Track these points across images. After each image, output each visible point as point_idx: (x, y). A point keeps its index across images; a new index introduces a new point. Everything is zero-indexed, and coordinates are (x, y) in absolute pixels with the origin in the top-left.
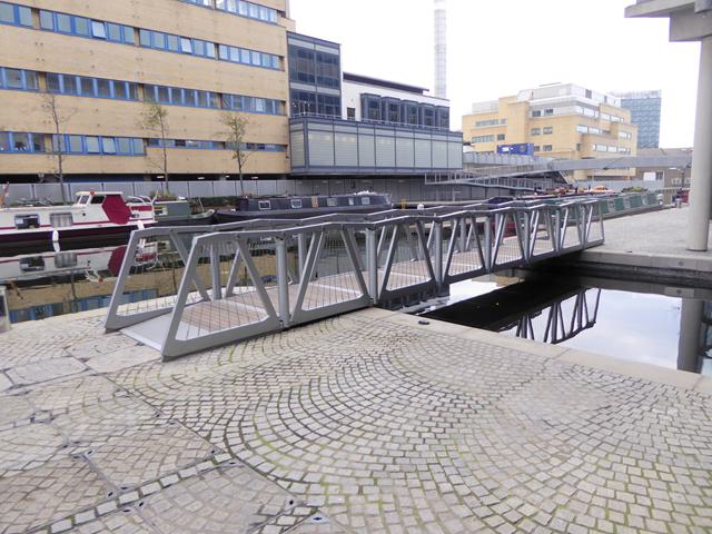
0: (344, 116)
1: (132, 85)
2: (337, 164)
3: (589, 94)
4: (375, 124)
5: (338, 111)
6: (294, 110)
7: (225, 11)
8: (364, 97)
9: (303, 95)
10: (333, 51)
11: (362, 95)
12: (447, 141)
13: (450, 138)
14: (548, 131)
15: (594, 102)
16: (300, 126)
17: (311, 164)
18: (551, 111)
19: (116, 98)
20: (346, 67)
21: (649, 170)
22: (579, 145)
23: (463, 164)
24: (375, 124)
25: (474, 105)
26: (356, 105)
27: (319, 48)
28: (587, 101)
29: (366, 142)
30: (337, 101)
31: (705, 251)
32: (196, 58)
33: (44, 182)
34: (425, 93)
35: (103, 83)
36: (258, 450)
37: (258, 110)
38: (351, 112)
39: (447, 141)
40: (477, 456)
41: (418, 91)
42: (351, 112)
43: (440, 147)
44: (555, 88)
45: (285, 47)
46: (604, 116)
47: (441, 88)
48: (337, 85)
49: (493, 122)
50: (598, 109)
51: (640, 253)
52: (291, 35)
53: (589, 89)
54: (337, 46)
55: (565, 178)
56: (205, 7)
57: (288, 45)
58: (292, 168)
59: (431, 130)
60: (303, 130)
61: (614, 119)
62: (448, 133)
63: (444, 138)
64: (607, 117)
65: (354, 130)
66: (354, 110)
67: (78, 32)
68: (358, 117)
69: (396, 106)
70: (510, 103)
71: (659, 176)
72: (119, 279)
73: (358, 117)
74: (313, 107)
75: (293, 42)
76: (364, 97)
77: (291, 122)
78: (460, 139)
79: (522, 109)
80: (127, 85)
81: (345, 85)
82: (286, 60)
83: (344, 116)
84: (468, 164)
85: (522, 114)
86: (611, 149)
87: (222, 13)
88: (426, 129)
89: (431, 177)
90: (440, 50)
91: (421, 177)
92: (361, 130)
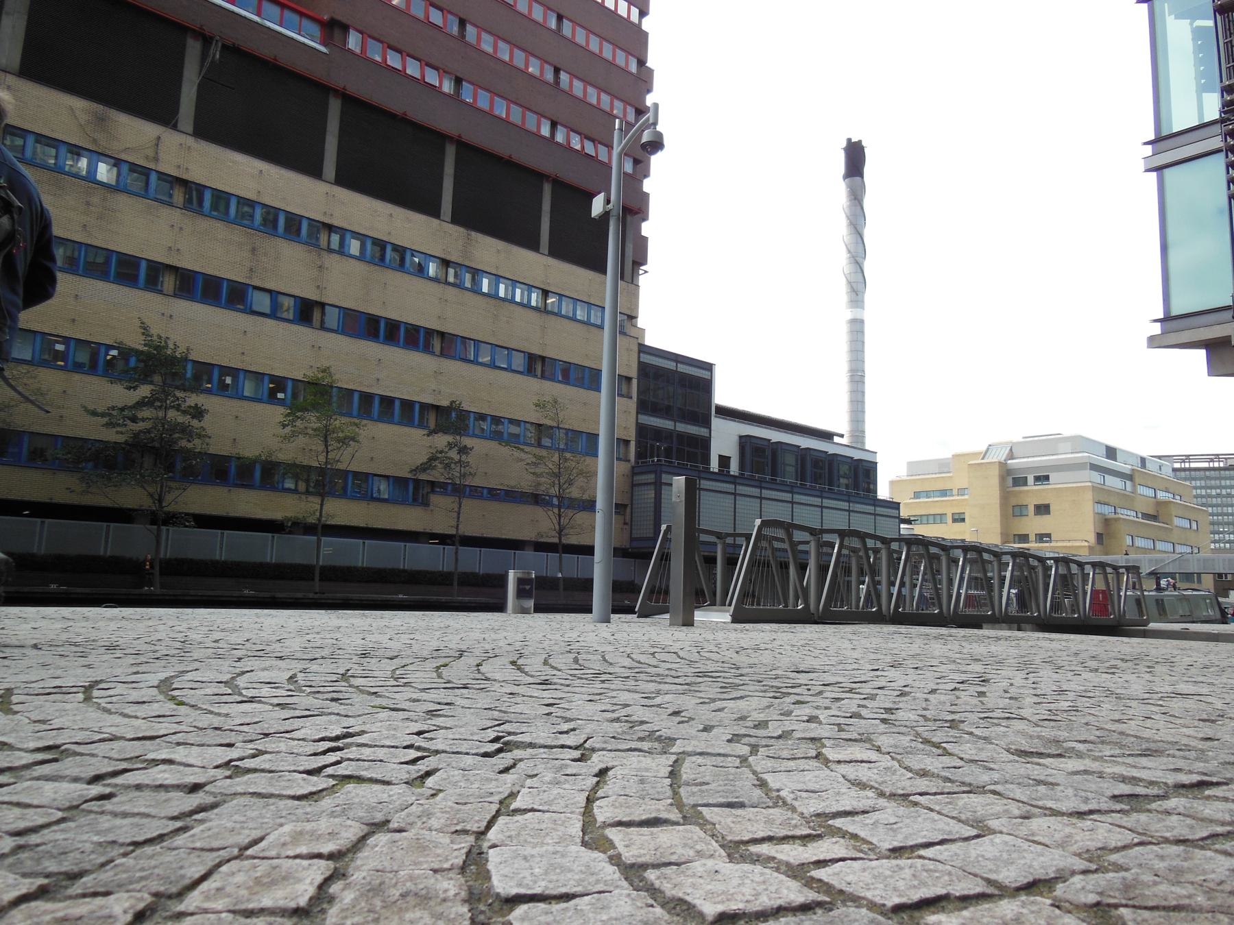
0: (714, 465)
1: (425, 407)
3: (1111, 452)
4: (761, 481)
5: (706, 459)
6: (639, 455)
7: (558, 315)
8: (744, 441)
9: (658, 433)
10: (703, 374)
11: (741, 437)
12: (875, 515)
13: (879, 510)
14: (1043, 509)
16: (651, 478)
18: (1047, 478)
19: (400, 423)
20: (723, 395)
24: (822, 491)
25: (910, 464)
26: (732, 451)
27: (682, 368)
28: (1109, 463)
30: (705, 444)
32: (479, 368)
33: (290, 533)
34: (836, 439)
35: (387, 402)
37: (246, 393)
38: (724, 461)
39: (875, 515)
41: (827, 436)
42: (724, 461)
44: (1051, 443)
45: (635, 366)
46: (1142, 490)
47: (858, 432)
48: (707, 424)
49: (944, 493)
50: (1130, 477)
52: (643, 349)
53: (1112, 443)
54: (709, 367)
56: (579, 321)
57: (639, 362)
58: (632, 539)
59: (761, 481)
60: (655, 483)
61: (1162, 495)
63: (870, 509)
65: (729, 487)
67: (327, 325)
68: (734, 468)
69: (763, 451)
70: (972, 463)
72: (1141, 520)
73: (734, 468)
74: (668, 453)
75: (646, 359)
76: (744, 441)
77: (634, 472)
78: (893, 512)
79: (995, 473)
80: (417, 407)
81: (717, 423)
82: (635, 382)
83: (714, 465)
85: (995, 481)
86: (1160, 546)
87: (553, 318)
88: (812, 488)
90: (857, 379)
92: (742, 489)
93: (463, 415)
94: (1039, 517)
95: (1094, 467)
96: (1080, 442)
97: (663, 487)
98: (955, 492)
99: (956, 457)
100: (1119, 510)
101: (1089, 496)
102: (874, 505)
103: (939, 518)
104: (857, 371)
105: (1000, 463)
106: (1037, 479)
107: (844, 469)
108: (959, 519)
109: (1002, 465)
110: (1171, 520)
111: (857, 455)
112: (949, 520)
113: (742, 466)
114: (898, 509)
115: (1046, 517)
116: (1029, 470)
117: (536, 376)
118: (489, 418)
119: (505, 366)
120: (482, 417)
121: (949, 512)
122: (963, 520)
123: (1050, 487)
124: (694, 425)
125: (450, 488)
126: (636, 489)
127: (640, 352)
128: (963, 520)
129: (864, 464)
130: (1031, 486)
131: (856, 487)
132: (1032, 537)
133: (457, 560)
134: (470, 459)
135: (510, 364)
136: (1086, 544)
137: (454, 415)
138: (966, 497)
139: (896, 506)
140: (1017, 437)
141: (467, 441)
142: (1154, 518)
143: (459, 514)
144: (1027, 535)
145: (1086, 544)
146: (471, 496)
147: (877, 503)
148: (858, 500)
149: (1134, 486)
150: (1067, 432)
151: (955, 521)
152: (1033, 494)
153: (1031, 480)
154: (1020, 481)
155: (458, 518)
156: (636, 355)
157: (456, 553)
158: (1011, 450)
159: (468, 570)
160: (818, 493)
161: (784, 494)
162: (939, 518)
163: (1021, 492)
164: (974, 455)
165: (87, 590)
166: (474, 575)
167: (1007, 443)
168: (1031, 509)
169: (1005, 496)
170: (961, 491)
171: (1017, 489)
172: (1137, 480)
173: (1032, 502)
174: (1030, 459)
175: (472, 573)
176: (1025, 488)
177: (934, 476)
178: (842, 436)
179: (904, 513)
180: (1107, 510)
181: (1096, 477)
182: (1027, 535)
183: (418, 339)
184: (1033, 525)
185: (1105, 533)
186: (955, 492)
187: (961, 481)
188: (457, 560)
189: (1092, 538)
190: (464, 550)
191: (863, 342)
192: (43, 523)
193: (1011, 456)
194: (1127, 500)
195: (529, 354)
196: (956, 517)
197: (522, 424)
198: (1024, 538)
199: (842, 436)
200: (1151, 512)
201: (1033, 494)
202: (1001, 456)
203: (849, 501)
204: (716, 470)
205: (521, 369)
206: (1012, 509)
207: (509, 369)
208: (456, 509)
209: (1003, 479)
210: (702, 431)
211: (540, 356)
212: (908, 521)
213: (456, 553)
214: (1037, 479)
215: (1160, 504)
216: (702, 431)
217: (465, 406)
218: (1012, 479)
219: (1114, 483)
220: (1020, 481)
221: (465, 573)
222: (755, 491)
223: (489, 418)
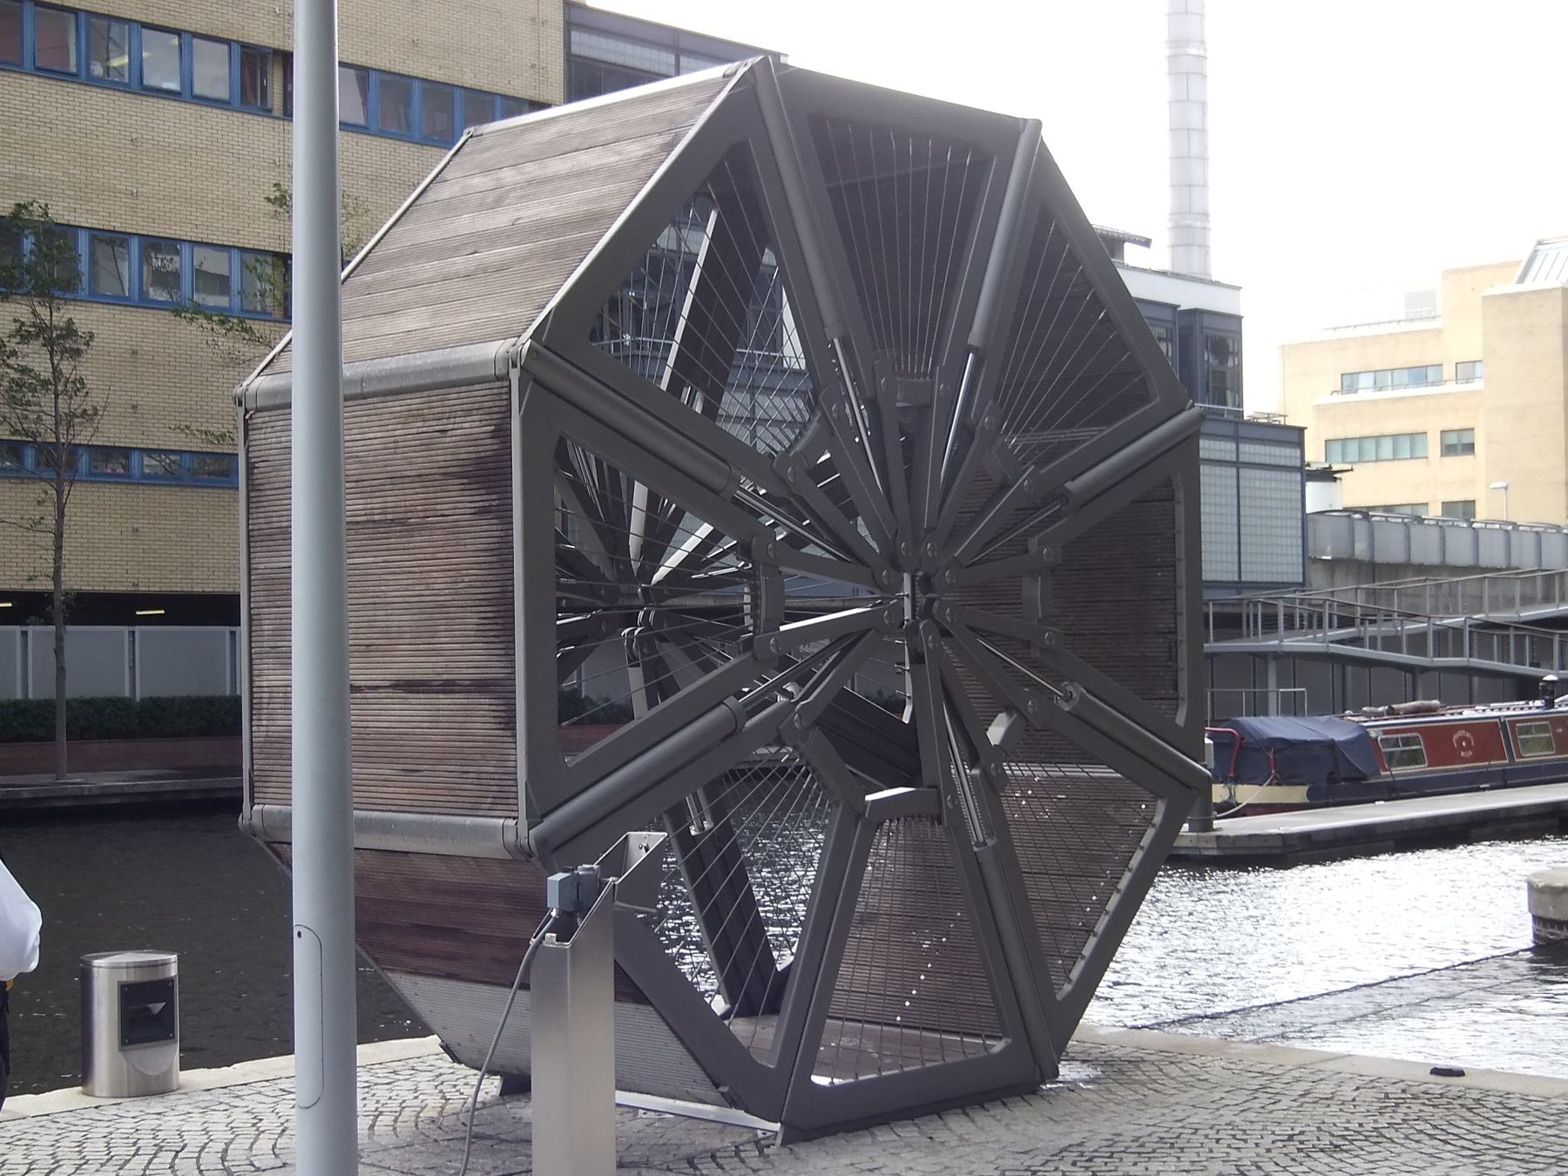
12: (1237, 465)
13: (1250, 451)
17: (1206, 576)
23: (1308, 560)
39: (1237, 465)
49: (1420, 374)
78: (1287, 455)
84: (1333, 565)
93: (58, 235)
97: (1243, 579)
98: (1449, 371)
102: (1237, 439)
103: (1407, 444)
104: (1187, 42)
105: (1563, 289)
108: (1458, 445)
111: (1187, 297)
112: (1434, 448)
114: (1300, 444)
117: (267, 112)
118: (135, 245)
119: (173, 85)
120: (111, 240)
121: (1433, 426)
122: (1469, 448)
125: (29, 457)
127: (569, 26)
128: (1469, 448)
129: (1207, 322)
133: (61, 670)
134: (87, 369)
135: (187, 78)
137: (28, 244)
138: (1477, 385)
139: (1295, 437)
141: (84, 317)
143: (59, 536)
146: (95, 477)
147: (1243, 432)
151: (1448, 450)
155: (59, 548)
156: (558, 37)
157: (59, 651)
159: (88, 693)
162: (1407, 444)
166: (119, 705)
170: (1465, 371)
175: (110, 701)
177: (1395, 328)
178: (1146, 243)
179: (1314, 455)
186: (1449, 371)
187: (1466, 341)
188: (61, 670)
190: (80, 635)
192: (24, 634)
195: (245, 46)
196: (1452, 439)
197: (186, 249)
199: (1146, 243)
205: (222, 92)
207: (186, 95)
208: (50, 521)
211: (276, 52)
212: (1327, 475)
213: (59, 651)
217: (61, 213)
221: (90, 702)
223: (135, 245)
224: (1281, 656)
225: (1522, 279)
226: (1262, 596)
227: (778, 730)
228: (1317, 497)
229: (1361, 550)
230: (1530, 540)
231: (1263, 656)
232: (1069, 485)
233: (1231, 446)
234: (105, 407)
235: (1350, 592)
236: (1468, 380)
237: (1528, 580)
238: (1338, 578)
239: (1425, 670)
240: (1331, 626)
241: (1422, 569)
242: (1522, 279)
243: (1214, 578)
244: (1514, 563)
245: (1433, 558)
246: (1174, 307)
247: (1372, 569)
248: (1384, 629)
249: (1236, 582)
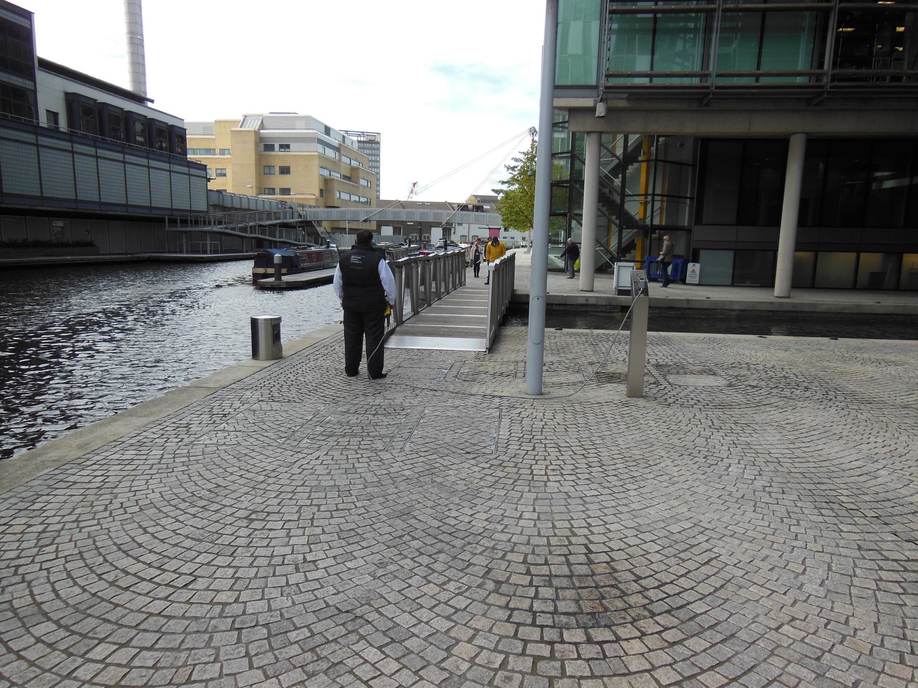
0: (43, 121)
2: (153, 205)
3: (328, 130)
8: (71, 100)
12: (189, 175)
13: (193, 171)
14: (285, 171)
15: (334, 141)
18: (288, 146)
21: (387, 223)
22: (321, 191)
23: (208, 205)
26: (60, 107)
29: (85, 165)
31: (592, 291)
36: (137, 526)
38: (53, 116)
39: (189, 175)
40: (272, 549)
42: (53, 116)
43: (160, 178)
44: (290, 119)
46: (345, 160)
48: (33, 78)
50: (337, 149)
51: (555, 294)
55: (318, 229)
61: (354, 163)
62: (37, 130)
63: (185, 170)
64: (347, 160)
66: (678, 264)
69: (163, 131)
71: (396, 231)
73: (63, 124)
76: (71, 100)
78: (202, 173)
81: (41, 76)
84: (215, 206)
85: (252, 146)
89: (173, 221)
91: (162, 220)
94: (282, 176)
95: (320, 142)
96: (309, 121)
99: (218, 122)
100: (332, 173)
101: (316, 162)
102: (36, 134)
105: (255, 131)
106: (281, 146)
107: (138, 127)
109: (257, 133)
110: (359, 181)
113: (71, 122)
115: (287, 176)
116: (276, 139)
122: (225, 175)
123: (290, 153)
124: (17, 76)
126: (594, 289)
128: (225, 175)
129: (156, 123)
130: (277, 152)
131: (151, 146)
132: (277, 191)
136: (314, 197)
140: (265, 111)
142: (349, 179)
144: (274, 189)
145: (314, 197)
148: (101, 145)
149: (340, 156)
150: (302, 113)
152: (278, 157)
153: (277, 147)
154: (269, 148)
158: (262, 122)
160: (120, 149)
161: (199, 171)
163: (270, 156)
164: (234, 122)
165: (148, 255)
167: (260, 115)
168: (277, 170)
169: (259, 158)
170: (223, 151)
171: (267, 153)
172: (342, 152)
173: (278, 164)
174: (277, 131)
176: (273, 153)
180: (326, 173)
181: (320, 148)
182: (274, 189)
183: (747, 143)
184: (279, 181)
185: (326, 187)
186: (217, 151)
187: (226, 143)
189: (317, 193)
191: (141, 6)
193: (262, 126)
194: (336, 164)
198: (272, 191)
200: (348, 175)
201: (278, 157)
202: (253, 126)
203: (148, 158)
204: (46, 126)
206: (264, 169)
209: (257, 145)
210: (28, 84)
214: (281, 146)
215: (354, 170)
216: (28, 84)
218: (265, 146)
219: (330, 153)
220: (269, 148)
222: (91, 151)
224: (211, 233)
225: (241, 127)
226: (201, 215)
227: (492, 348)
228: (212, 186)
229: (221, 204)
230: (262, 202)
231: (205, 232)
232: (361, 180)
233: (146, 160)
234: (289, 536)
235: (219, 214)
236: (224, 155)
237: (261, 213)
238: (217, 211)
239: (246, 237)
240: (215, 224)
241: (236, 209)
242: (241, 127)
243: (133, 203)
244: (258, 208)
245: (238, 206)
246: (146, 117)
247: (224, 208)
248: (231, 226)
249: (35, 197)
